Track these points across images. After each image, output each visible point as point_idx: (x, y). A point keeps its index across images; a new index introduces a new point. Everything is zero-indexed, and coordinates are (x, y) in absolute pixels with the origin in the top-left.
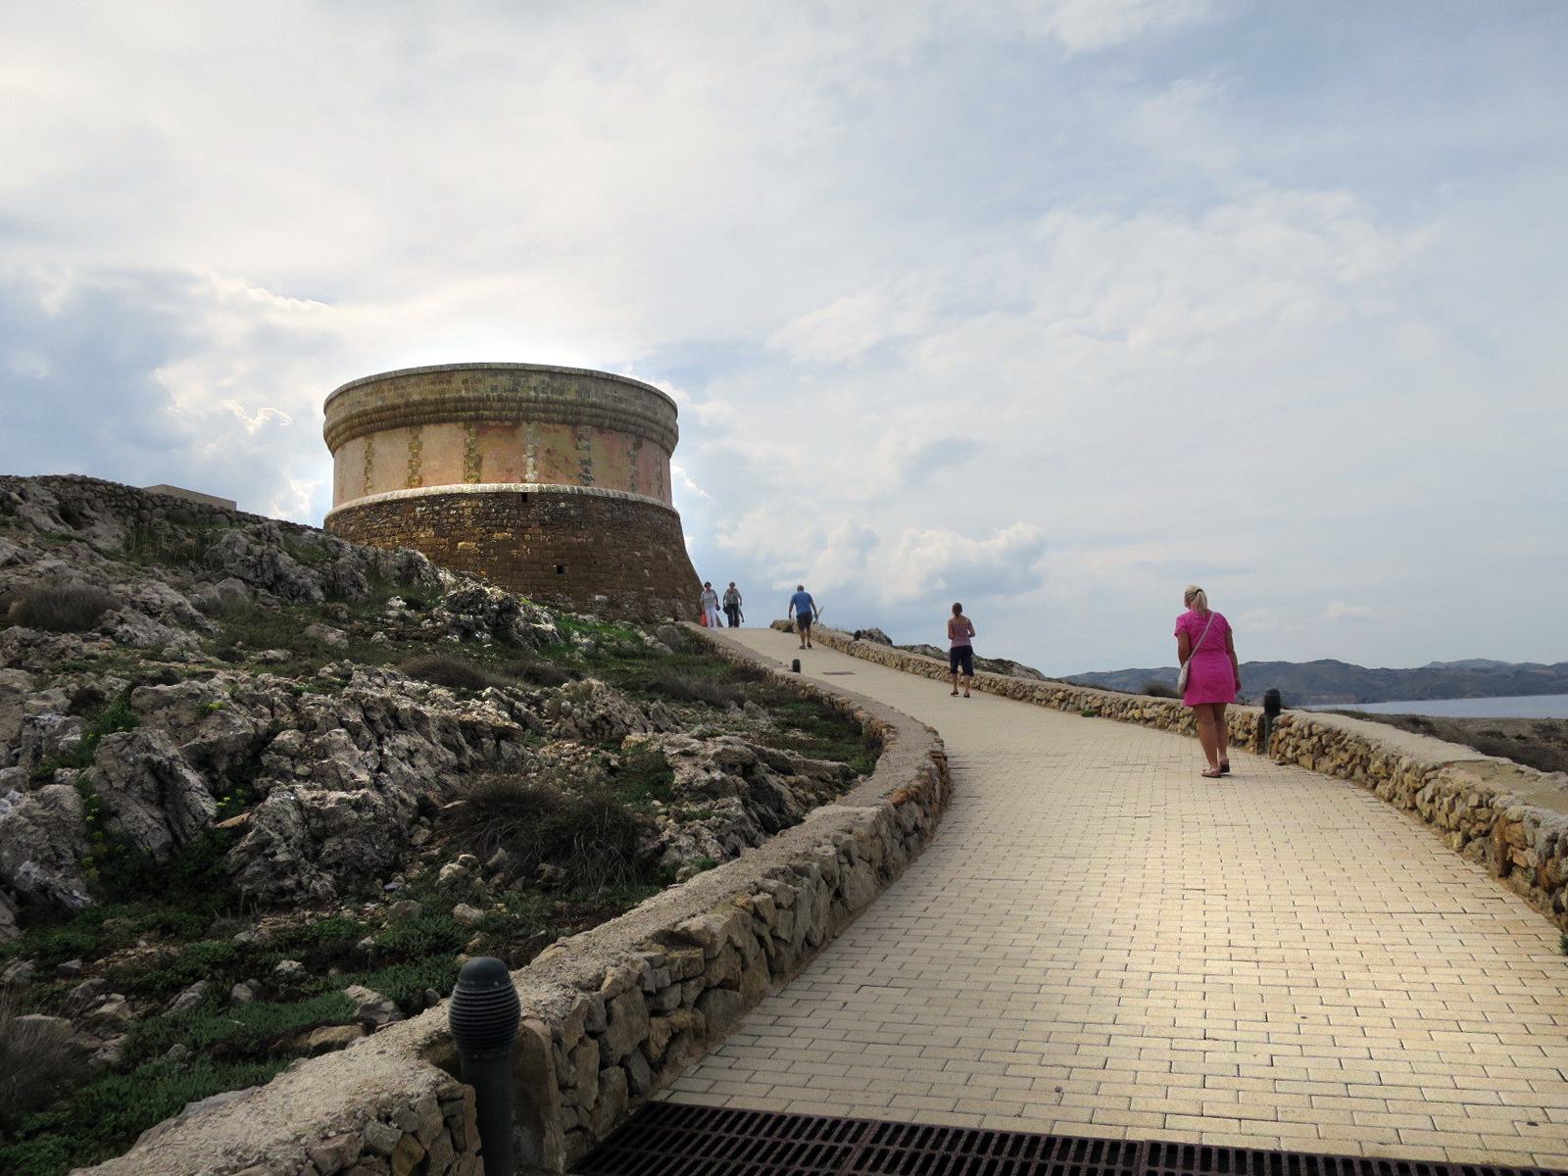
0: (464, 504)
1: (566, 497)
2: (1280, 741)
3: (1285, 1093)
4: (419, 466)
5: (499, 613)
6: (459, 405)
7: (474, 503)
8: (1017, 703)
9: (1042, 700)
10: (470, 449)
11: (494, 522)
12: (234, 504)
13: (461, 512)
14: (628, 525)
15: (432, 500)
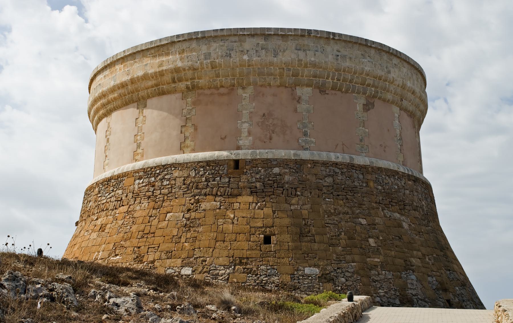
1: (283, 163)
10: (187, 119)
11: (203, 191)
13: (173, 182)
14: (353, 190)
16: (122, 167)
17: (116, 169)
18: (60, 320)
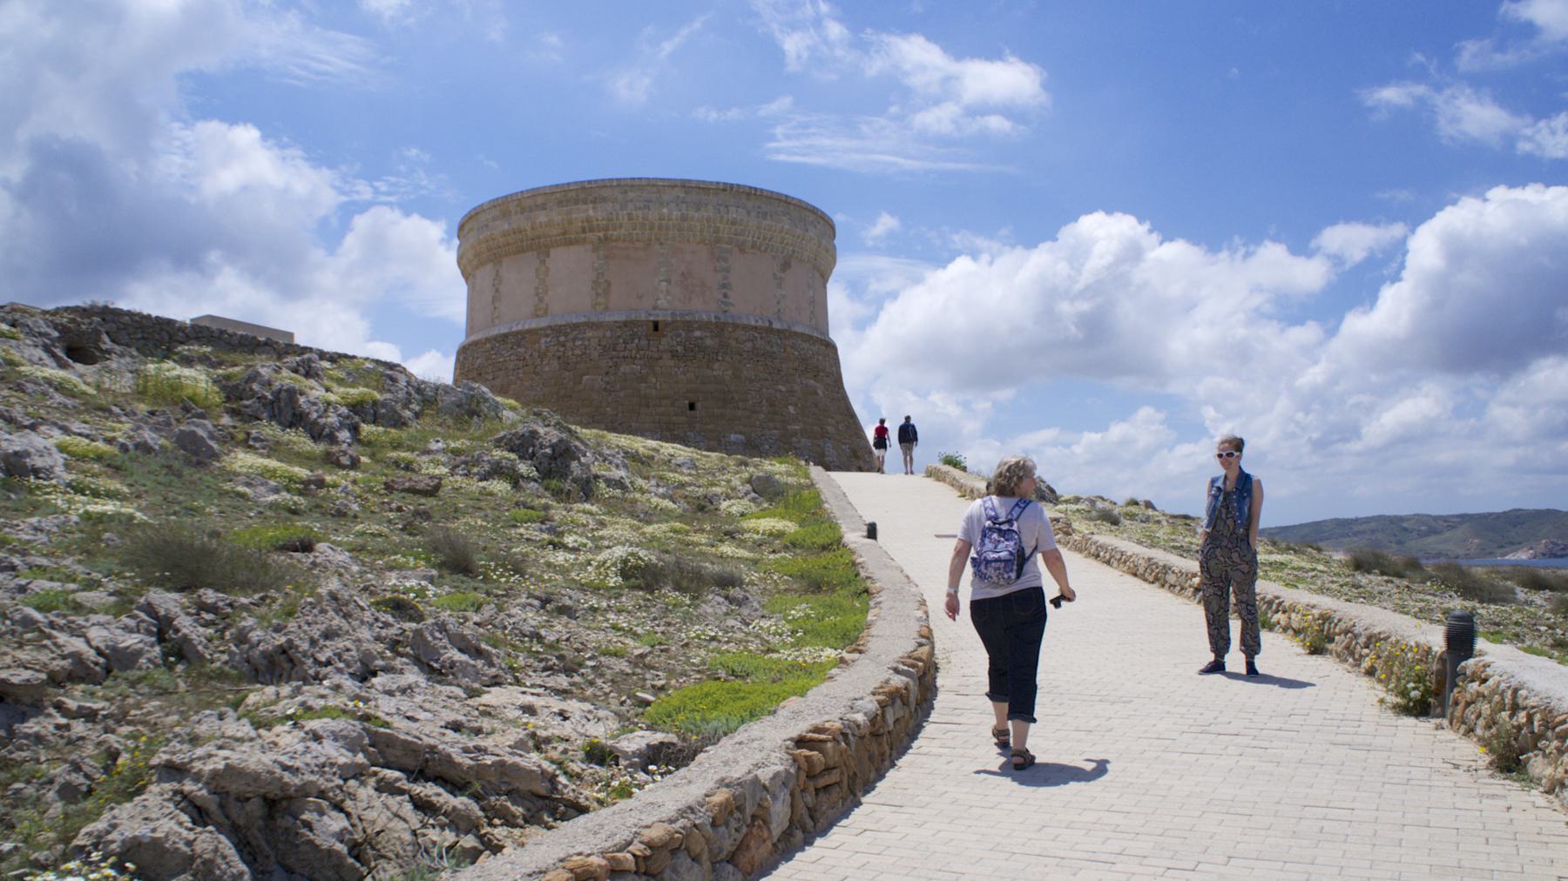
0: (591, 334)
2: (1468, 704)
4: (546, 292)
5: (553, 457)
7: (600, 333)
8: (1146, 585)
9: (1175, 586)
12: (291, 335)
13: (587, 343)
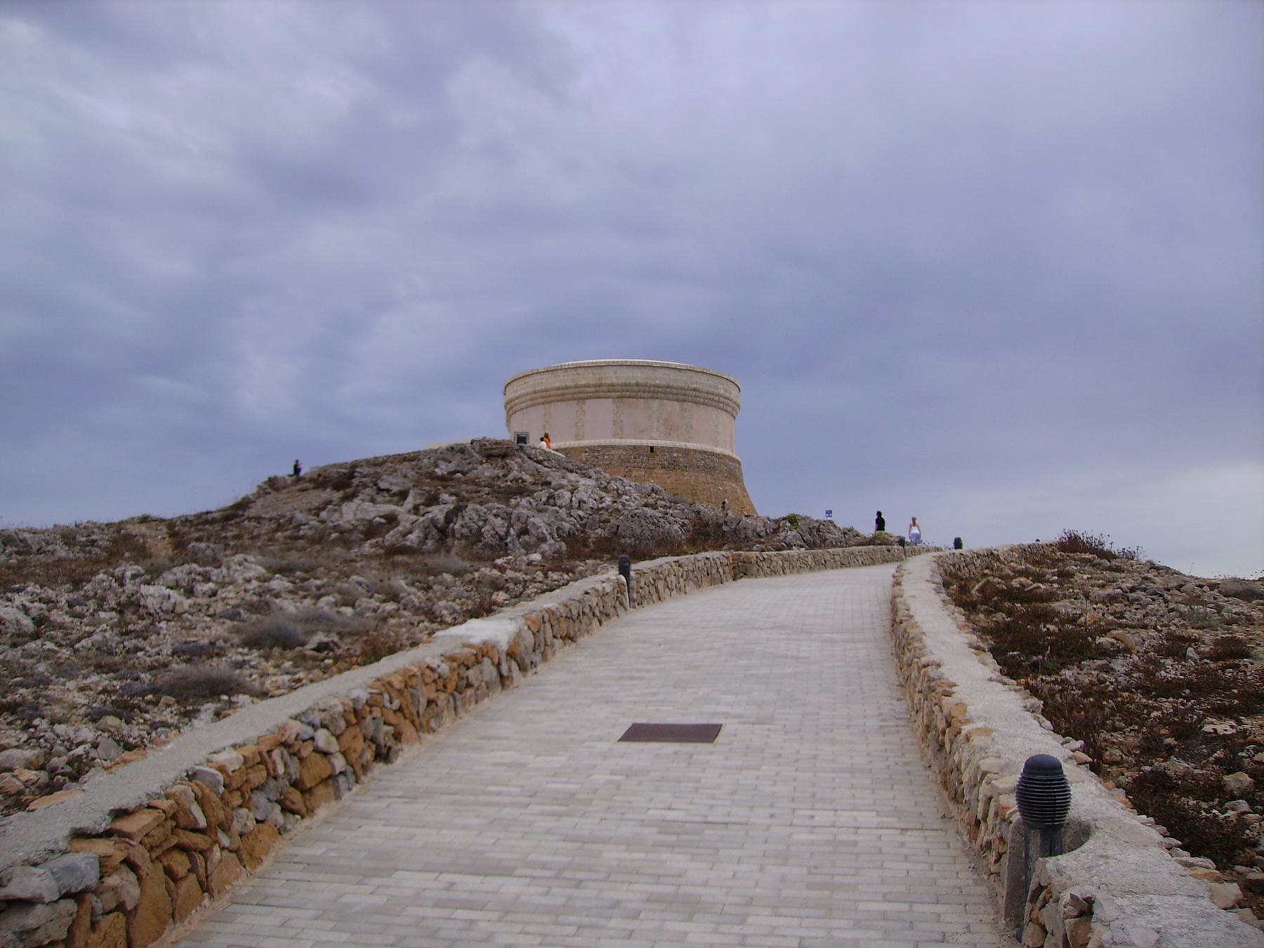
1: (679, 450)
3: (912, 829)
6: (611, 388)
14: (714, 468)
15: (592, 449)
16: (568, 443)
17: (562, 443)
18: (715, 533)
